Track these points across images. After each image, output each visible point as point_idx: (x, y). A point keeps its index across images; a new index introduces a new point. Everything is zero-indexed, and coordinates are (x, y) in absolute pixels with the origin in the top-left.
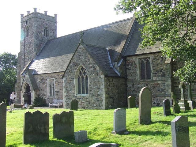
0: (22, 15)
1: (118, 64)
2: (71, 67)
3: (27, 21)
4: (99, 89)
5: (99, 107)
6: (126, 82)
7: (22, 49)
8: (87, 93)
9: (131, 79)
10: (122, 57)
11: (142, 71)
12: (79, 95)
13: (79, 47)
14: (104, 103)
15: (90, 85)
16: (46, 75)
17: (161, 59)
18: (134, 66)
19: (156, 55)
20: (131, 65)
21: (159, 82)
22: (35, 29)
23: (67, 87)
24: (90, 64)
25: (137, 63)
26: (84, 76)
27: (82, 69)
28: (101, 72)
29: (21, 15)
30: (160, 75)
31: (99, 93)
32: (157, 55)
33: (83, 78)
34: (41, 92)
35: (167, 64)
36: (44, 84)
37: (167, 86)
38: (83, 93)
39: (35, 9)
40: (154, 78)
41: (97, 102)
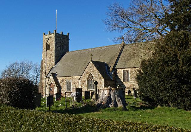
6: (116, 83)
21: (133, 84)
26: (92, 79)
39: (62, 32)
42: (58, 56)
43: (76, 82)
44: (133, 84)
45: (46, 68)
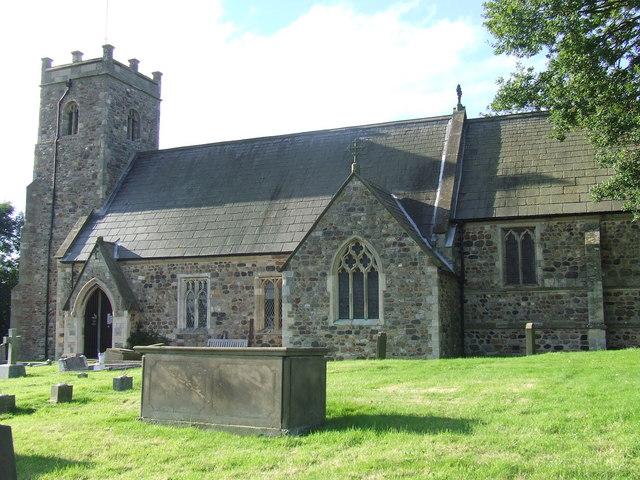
0: (47, 62)
1: (446, 240)
2: (316, 240)
3: (70, 84)
4: (419, 305)
5: (419, 354)
6: (462, 289)
7: (46, 173)
8: (373, 314)
9: (477, 283)
10: (452, 222)
11: (510, 259)
12: (343, 323)
13: (350, 184)
14: (435, 342)
15: (386, 295)
16: (174, 262)
17: (567, 234)
18: (487, 248)
19: (554, 223)
20: (477, 245)
21: (561, 293)
22: (106, 111)
23: (298, 300)
24: (388, 235)
25: (498, 241)
26: (363, 270)
27: (357, 247)
28: (426, 258)
29: (43, 59)
30: (564, 273)
31: (418, 317)
32: (555, 223)
33: (357, 274)
34: (148, 315)
35: (591, 247)
36: (161, 290)
37: (594, 300)
38: (358, 315)
39: (108, 49)
40: (546, 281)
41: (410, 341)
42: (118, 166)
43: (234, 287)
44: (561, 293)
45: (53, 216)
